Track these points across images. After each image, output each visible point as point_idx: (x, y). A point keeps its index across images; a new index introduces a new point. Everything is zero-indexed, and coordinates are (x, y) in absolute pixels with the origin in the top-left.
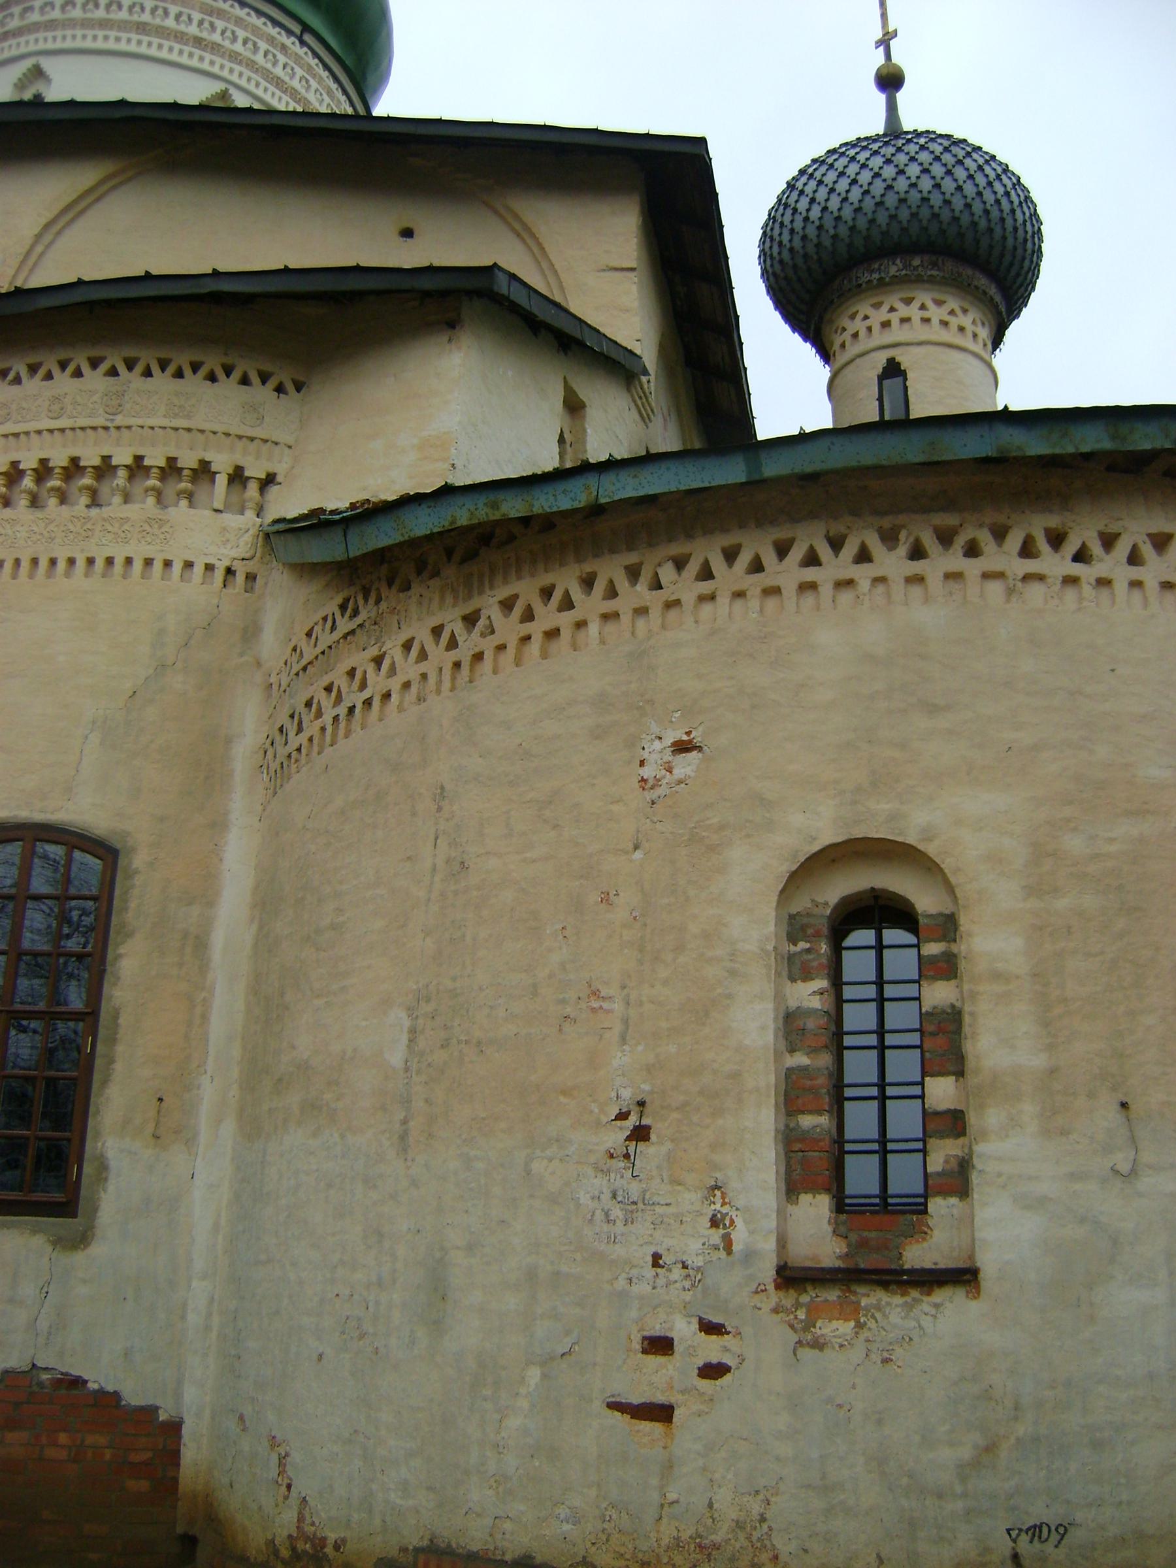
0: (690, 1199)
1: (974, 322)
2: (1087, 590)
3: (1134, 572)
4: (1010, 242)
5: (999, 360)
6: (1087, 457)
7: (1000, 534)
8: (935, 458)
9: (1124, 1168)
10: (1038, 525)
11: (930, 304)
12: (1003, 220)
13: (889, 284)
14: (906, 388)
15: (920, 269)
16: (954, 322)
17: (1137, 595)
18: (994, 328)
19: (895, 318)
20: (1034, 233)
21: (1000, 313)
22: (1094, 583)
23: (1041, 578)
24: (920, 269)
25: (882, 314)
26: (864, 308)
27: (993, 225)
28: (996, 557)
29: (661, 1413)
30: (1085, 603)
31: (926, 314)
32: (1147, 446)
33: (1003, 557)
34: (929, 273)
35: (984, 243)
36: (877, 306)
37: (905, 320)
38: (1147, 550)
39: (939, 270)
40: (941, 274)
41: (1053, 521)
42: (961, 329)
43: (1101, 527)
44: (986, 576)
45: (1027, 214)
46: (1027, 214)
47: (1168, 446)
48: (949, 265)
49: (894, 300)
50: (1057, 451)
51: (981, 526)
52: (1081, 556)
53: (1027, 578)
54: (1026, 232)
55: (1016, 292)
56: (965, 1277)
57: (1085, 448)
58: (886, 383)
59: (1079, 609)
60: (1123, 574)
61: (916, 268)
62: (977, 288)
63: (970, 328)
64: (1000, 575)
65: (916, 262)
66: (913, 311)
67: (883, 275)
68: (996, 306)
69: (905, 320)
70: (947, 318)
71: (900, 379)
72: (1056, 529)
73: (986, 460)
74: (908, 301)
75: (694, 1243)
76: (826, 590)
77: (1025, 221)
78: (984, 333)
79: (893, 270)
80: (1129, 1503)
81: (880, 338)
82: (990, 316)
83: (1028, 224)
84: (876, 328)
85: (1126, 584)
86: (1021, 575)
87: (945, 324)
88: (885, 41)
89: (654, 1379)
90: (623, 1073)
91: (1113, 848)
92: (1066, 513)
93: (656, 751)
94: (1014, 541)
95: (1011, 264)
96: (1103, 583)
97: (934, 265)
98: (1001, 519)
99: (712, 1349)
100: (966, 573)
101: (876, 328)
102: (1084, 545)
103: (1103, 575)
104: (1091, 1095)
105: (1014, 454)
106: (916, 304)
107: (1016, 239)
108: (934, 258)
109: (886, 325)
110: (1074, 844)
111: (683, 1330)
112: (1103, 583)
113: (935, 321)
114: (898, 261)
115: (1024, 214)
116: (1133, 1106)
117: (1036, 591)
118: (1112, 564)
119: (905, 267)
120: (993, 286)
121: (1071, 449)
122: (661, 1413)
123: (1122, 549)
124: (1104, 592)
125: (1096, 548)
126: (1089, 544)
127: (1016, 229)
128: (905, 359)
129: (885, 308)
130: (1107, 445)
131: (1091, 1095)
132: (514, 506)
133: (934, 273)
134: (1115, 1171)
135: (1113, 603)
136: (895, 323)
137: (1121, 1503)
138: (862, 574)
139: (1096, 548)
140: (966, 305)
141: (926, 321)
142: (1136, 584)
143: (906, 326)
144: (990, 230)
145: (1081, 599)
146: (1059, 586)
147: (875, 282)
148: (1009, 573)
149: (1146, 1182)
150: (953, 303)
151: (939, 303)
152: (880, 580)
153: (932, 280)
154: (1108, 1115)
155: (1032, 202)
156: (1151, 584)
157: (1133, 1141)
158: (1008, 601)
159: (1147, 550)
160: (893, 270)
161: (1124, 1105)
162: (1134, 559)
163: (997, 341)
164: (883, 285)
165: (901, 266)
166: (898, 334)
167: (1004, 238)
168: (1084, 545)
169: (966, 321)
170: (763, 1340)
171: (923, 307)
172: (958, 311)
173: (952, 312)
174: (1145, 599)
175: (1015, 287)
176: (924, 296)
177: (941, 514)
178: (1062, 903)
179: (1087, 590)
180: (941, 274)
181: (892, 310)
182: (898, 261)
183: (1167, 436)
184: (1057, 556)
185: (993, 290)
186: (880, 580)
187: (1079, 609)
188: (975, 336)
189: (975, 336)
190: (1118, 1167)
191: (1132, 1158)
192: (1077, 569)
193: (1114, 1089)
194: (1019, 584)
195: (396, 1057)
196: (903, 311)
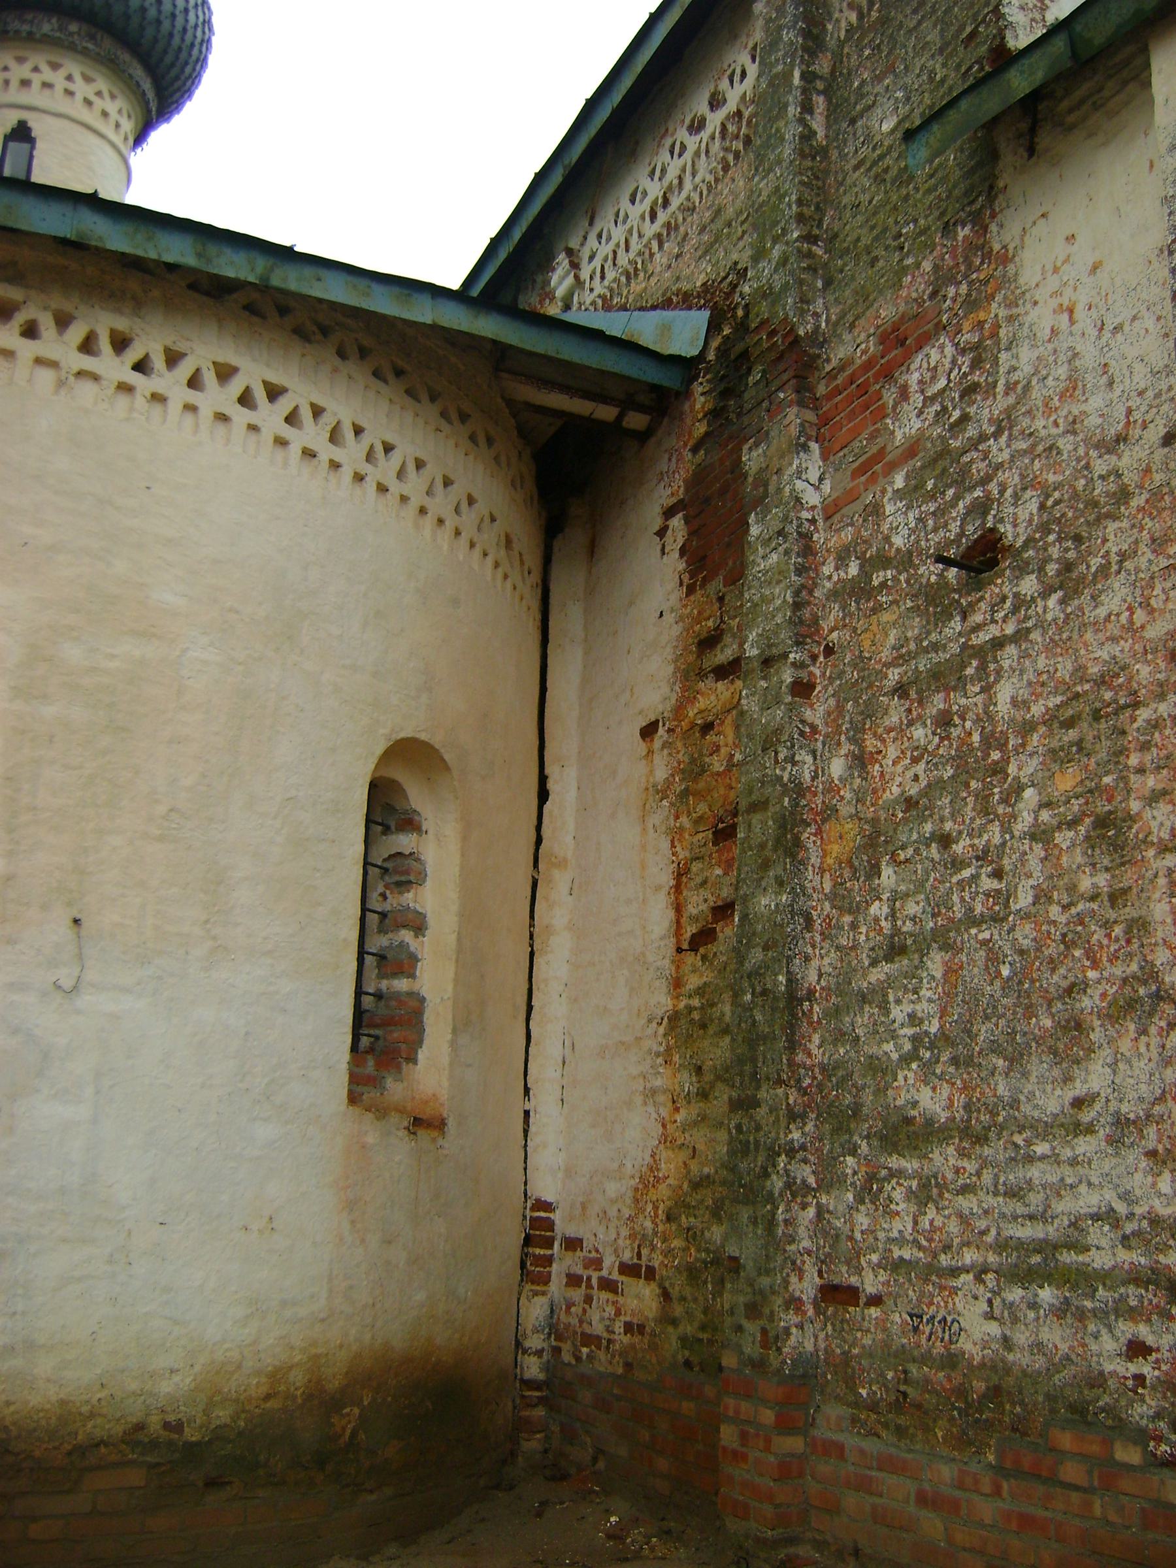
1: (120, 111)
2: (140, 401)
3: (192, 396)
4: (176, 40)
5: (139, 160)
6: (172, 267)
7: (63, 322)
8: (10, 224)
9: (67, 983)
10: (105, 322)
11: (78, 77)
12: (173, 16)
13: (40, 41)
14: (31, 157)
15: (76, 37)
16: (99, 103)
17: (189, 418)
18: (140, 126)
19: (36, 79)
20: (203, 41)
21: (149, 111)
22: (149, 396)
23: (96, 378)
24: (76, 37)
25: (24, 71)
27: (162, 18)
28: (51, 344)
30: (135, 415)
31: (71, 87)
32: (230, 273)
33: (61, 347)
34: (85, 44)
35: (150, 32)
36: (21, 60)
37: (47, 85)
38: (209, 377)
39: (96, 44)
40: (97, 50)
41: (122, 324)
42: (105, 114)
43: (169, 343)
44: (39, 361)
45: (201, 19)
46: (201, 19)
47: (251, 279)
48: (108, 43)
49: (39, 59)
50: (140, 253)
51: (45, 308)
52: (141, 367)
53: (80, 374)
54: (195, 37)
55: (171, 96)
57: (169, 258)
58: (11, 145)
59: (127, 419)
60: (179, 394)
61: (71, 34)
62: (131, 76)
63: (114, 115)
64: (54, 365)
65: (73, 27)
66: (58, 79)
67: (34, 29)
68: (147, 103)
69: (47, 85)
70: (93, 98)
71: (26, 146)
72: (123, 333)
73: (64, 242)
74: (55, 66)
76: (295, 450)
77: (196, 26)
78: (128, 126)
79: (46, 28)
80: (23, 1313)
82: (138, 109)
83: (199, 30)
84: (14, 84)
85: (181, 406)
86: (75, 369)
87: (88, 103)
91: (114, 664)
92: (136, 319)
94: (76, 333)
95: (173, 65)
96: (157, 398)
97: (92, 37)
98: (68, 307)
100: (19, 354)
101: (14, 84)
102: (147, 356)
103: (160, 391)
104: (45, 907)
105: (94, 243)
106: (62, 73)
107: (183, 40)
108: (93, 30)
109: (25, 83)
110: (73, 653)
112: (157, 398)
113: (79, 97)
114: (54, 20)
115: (197, 17)
116: (85, 923)
117: (87, 388)
118: (172, 383)
119: (60, 29)
120: (149, 81)
121: (153, 255)
123: (185, 370)
124: (157, 408)
125: (159, 362)
126: (153, 356)
127: (185, 30)
128: (38, 125)
129: (28, 66)
130: (190, 260)
131: (45, 907)
133: (90, 46)
134: (57, 986)
135: (165, 421)
136: (36, 85)
137: (15, 1313)
138: (241, 416)
139: (159, 362)
140: (116, 91)
141: (69, 93)
142: (191, 408)
143: (47, 92)
144: (159, 22)
145: (131, 409)
146: (112, 390)
147: (24, 34)
148: (63, 364)
149: (86, 1000)
150: (102, 84)
151: (87, 79)
152: (253, 428)
153: (85, 52)
154: (61, 930)
155: (209, 9)
156: (206, 412)
157: (80, 957)
158: (56, 392)
159: (209, 377)
160: (46, 28)
161: (76, 921)
162: (194, 382)
163: (140, 139)
164: (32, 40)
165: (56, 26)
166: (34, 96)
167: (171, 35)
168: (147, 356)
169: (112, 107)
171: (69, 78)
172: (106, 94)
173: (99, 94)
174: (197, 425)
175: (171, 89)
176: (73, 67)
177: (6, 285)
178: (49, 711)
179: (140, 401)
180: (97, 50)
181: (36, 69)
182: (54, 20)
183: (252, 270)
184: (117, 360)
185: (147, 85)
186: (253, 428)
187: (127, 419)
188: (118, 126)
189: (118, 126)
190: (60, 983)
191: (76, 974)
192: (135, 378)
193: (69, 904)
194: (72, 378)
196: (48, 74)
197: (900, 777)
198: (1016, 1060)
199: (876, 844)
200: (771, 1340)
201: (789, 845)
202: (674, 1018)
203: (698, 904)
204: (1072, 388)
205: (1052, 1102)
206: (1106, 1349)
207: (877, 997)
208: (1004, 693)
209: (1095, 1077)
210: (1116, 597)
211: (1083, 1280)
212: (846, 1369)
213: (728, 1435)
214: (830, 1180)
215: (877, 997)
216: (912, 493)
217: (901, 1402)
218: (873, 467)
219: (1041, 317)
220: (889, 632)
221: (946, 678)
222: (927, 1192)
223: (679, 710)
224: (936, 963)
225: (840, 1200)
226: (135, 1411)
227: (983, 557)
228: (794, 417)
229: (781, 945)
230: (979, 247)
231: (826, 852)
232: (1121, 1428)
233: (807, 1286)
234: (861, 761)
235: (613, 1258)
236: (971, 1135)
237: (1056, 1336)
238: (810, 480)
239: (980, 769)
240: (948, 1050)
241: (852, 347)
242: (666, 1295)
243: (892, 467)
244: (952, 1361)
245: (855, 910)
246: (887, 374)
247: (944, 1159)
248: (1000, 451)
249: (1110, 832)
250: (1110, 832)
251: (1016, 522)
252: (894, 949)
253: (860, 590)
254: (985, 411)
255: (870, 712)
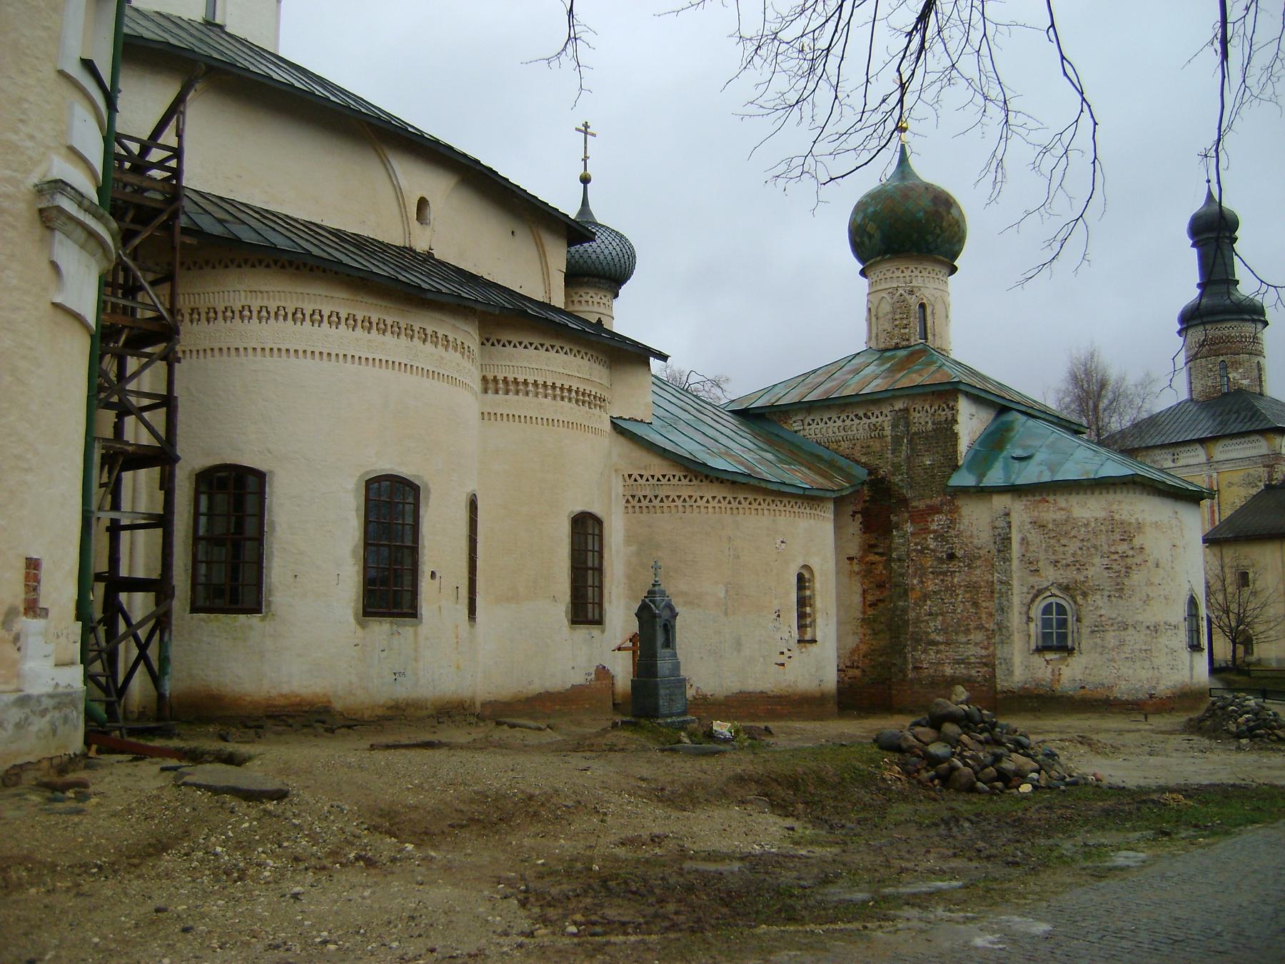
0: (786, 629)
26: (592, 293)
29: (783, 665)
49: (601, 294)
56: (814, 641)
75: (786, 636)
81: (596, 308)
88: (585, 159)
89: (782, 659)
90: (776, 604)
93: (778, 541)
99: (789, 654)
111: (785, 651)
122: (783, 665)
132: (763, 485)
170: (795, 652)
195: (722, 595)
197: (931, 587)
198: (957, 634)
199: (926, 597)
200: (905, 676)
201: (906, 592)
202: (863, 620)
203: (870, 598)
204: (971, 536)
205: (964, 640)
206: (973, 673)
207: (927, 622)
208: (956, 580)
209: (972, 637)
210: (978, 572)
211: (970, 663)
212: (920, 680)
213: (894, 692)
214: (914, 649)
215: (927, 622)
216: (935, 539)
217: (932, 683)
218: (926, 530)
219: (966, 522)
220: (929, 562)
221: (944, 573)
222: (938, 652)
223: (862, 557)
224: (940, 618)
225: (917, 654)
226: (725, 694)
227: (952, 557)
228: (906, 515)
229: (905, 611)
230: (951, 502)
231: (913, 596)
232: (975, 682)
233: (910, 666)
234: (922, 582)
235: (609, 735)
236: (947, 644)
237: (964, 671)
238: (909, 528)
239: (951, 590)
240: (944, 630)
241: (921, 505)
242: (864, 671)
243: (930, 533)
244: (943, 676)
245: (921, 607)
246: (929, 514)
247: (942, 647)
248: (956, 540)
249: (975, 604)
250: (975, 604)
251: (959, 553)
252: (930, 614)
253: (921, 552)
254: (953, 533)
255: (924, 574)
